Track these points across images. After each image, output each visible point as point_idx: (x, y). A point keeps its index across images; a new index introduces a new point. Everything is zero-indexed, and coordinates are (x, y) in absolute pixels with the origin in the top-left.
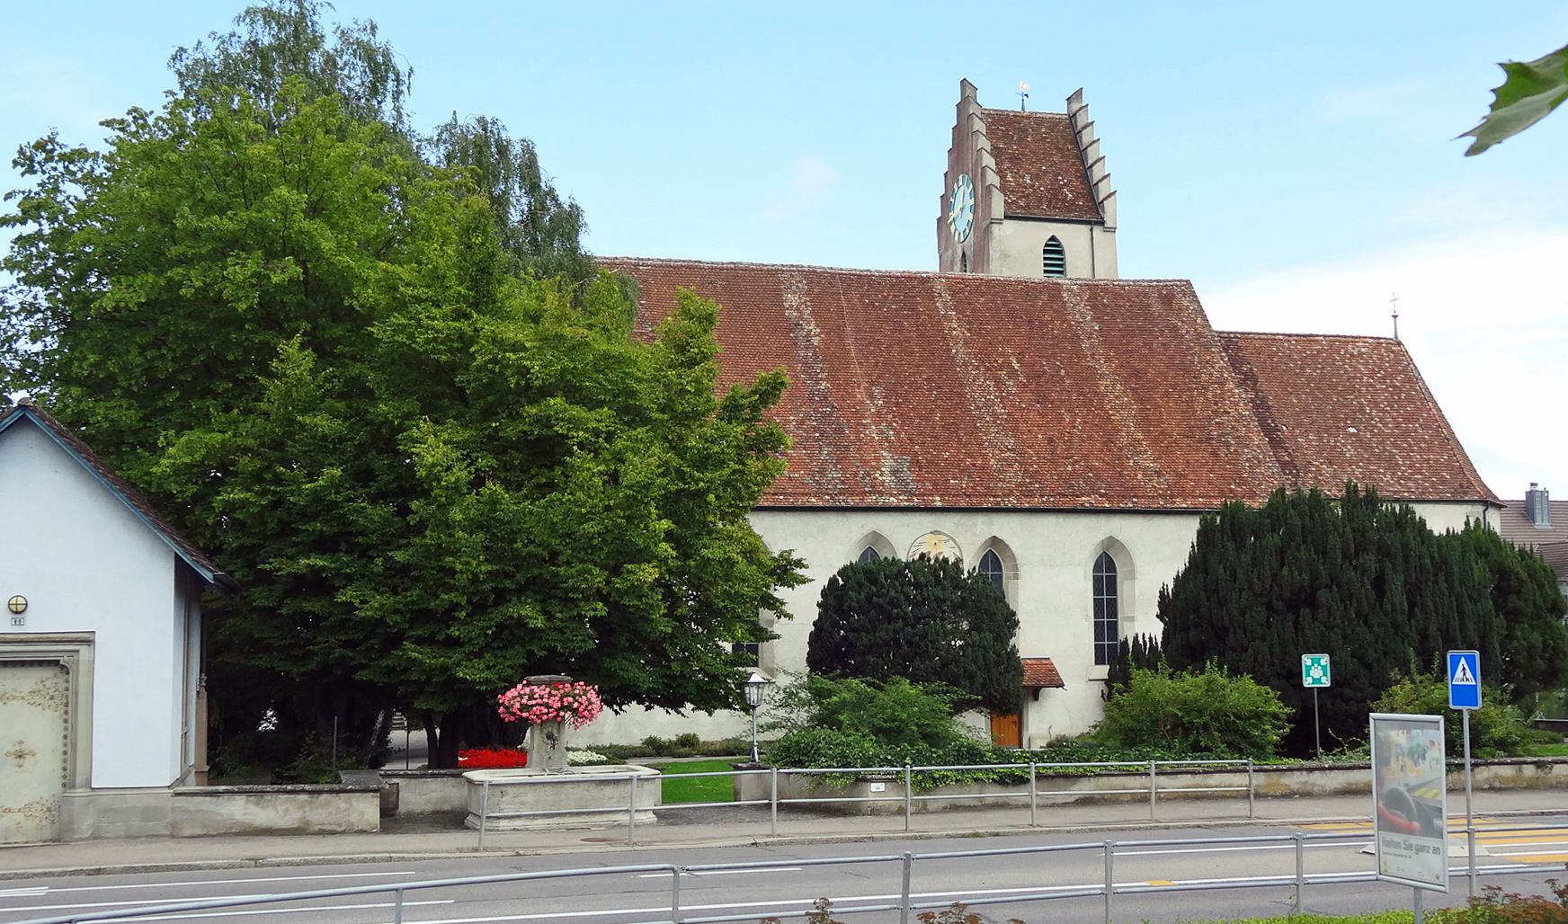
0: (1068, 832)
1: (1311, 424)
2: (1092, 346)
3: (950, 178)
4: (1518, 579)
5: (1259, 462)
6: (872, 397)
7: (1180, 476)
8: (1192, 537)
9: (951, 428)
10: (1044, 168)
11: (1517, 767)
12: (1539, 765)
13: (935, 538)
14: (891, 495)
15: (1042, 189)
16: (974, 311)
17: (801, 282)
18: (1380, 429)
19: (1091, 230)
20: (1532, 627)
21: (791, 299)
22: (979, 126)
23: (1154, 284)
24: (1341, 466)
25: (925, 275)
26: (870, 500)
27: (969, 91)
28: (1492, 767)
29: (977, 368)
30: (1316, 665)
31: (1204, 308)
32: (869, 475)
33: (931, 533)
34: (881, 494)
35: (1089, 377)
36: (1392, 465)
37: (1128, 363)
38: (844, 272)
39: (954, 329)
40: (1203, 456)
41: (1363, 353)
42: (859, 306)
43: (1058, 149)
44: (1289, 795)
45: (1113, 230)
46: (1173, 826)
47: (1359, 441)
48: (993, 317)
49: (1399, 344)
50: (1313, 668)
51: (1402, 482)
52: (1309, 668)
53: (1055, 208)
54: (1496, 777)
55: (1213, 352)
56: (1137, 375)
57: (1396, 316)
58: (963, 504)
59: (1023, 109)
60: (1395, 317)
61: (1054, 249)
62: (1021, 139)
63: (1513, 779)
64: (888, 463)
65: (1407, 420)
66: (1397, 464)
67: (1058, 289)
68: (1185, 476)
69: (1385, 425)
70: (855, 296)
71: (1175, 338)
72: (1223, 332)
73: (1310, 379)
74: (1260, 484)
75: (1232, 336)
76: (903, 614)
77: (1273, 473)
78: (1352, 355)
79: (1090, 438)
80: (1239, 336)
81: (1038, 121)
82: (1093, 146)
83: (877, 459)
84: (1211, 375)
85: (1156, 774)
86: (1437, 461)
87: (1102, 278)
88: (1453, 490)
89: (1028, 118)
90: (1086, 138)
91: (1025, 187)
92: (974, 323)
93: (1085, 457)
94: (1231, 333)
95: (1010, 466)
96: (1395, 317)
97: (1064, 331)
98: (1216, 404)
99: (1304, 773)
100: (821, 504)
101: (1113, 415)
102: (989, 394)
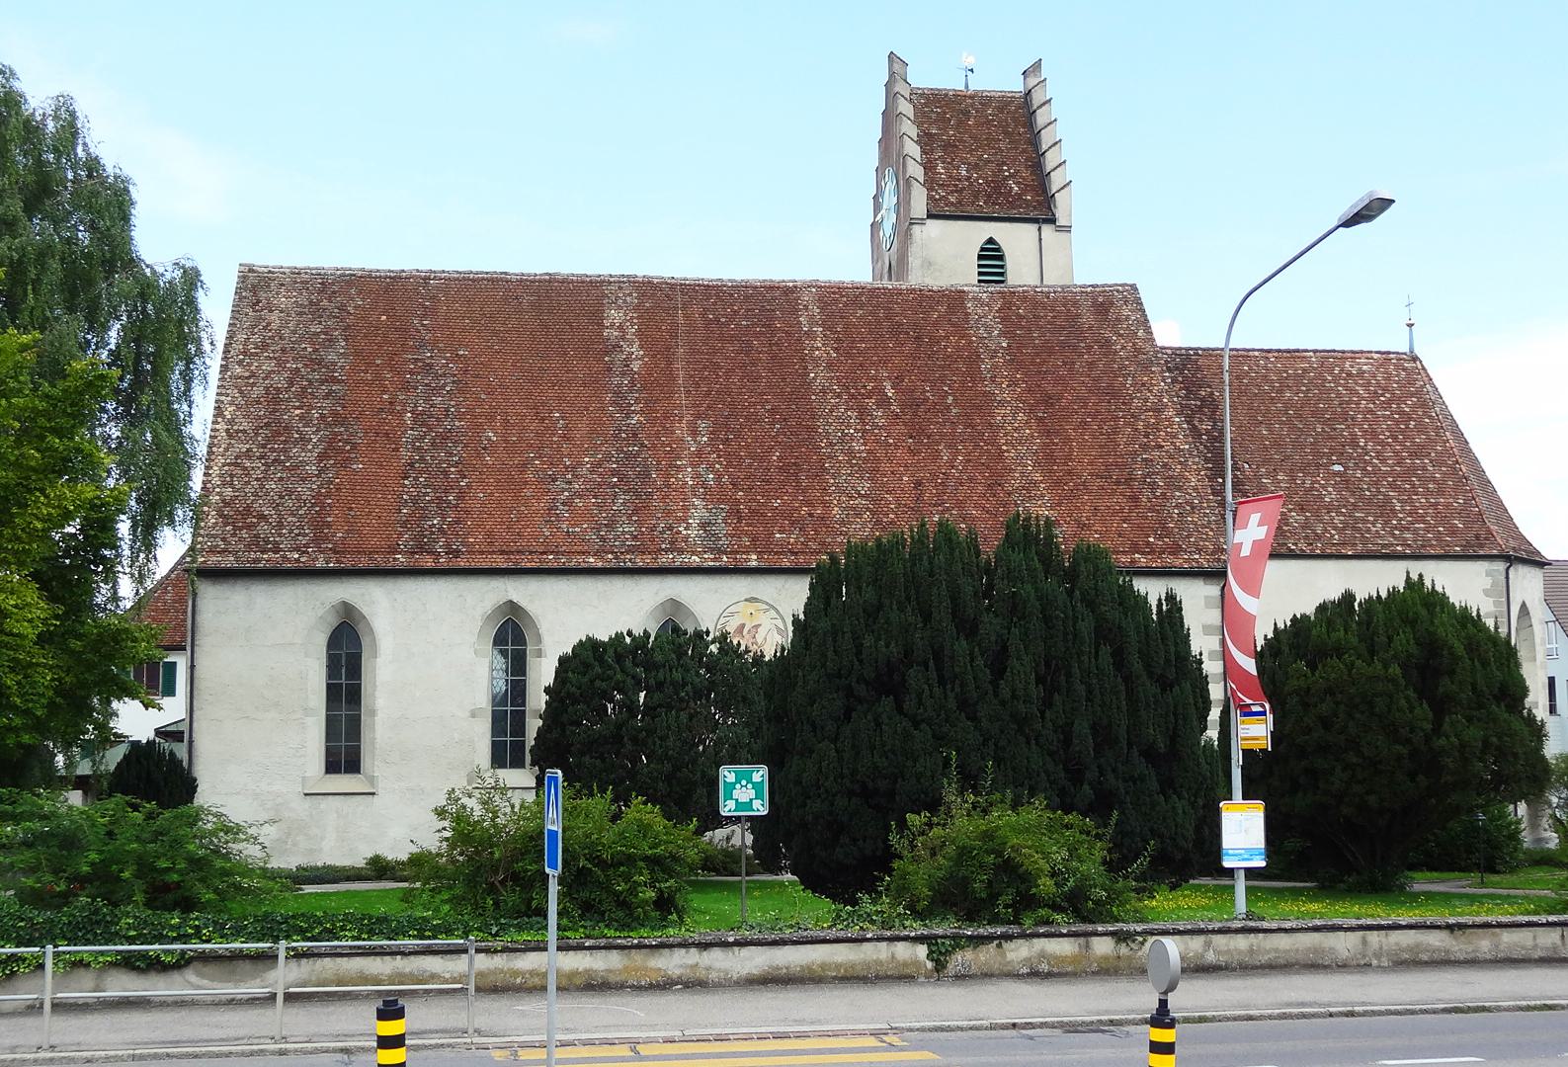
0: (89, 1061)
1: (1283, 460)
2: (995, 367)
3: (880, 172)
4: (1452, 654)
5: (1193, 508)
6: (694, 433)
7: (1082, 526)
8: (806, 593)
9: (790, 469)
10: (985, 156)
11: (1082, 940)
12: (1121, 937)
13: (751, 607)
14: (694, 553)
15: (981, 181)
16: (847, 326)
17: (630, 295)
18: (1374, 466)
19: (1040, 229)
20: (1469, 720)
21: (614, 315)
22: (905, 108)
23: (1089, 289)
24: (1316, 513)
25: (791, 284)
26: (665, 560)
27: (897, 67)
28: (1035, 940)
29: (839, 396)
30: (744, 782)
31: (1149, 317)
32: (670, 528)
33: (746, 600)
34: (681, 551)
35: (983, 405)
36: (1385, 511)
37: (1039, 386)
38: (687, 282)
39: (818, 349)
40: (1118, 501)
41: (1364, 372)
42: (700, 323)
43: (1006, 133)
44: (664, 985)
45: (1067, 229)
46: (296, 1051)
47: (1345, 481)
48: (870, 332)
49: (1415, 359)
50: (738, 786)
51: (1397, 532)
52: (731, 787)
53: (994, 204)
54: (1043, 955)
55: (1154, 372)
56: (1048, 401)
57: (1413, 325)
58: (786, 563)
59: (967, 86)
60: (1410, 326)
61: (991, 255)
62: (960, 123)
63: (1074, 960)
64: (699, 511)
65: (1413, 455)
66: (1393, 510)
67: (960, 297)
68: (1090, 527)
69: (1383, 461)
70: (696, 311)
71: (1105, 355)
72: (1180, 349)
73: (1288, 404)
74: (1189, 536)
75: (1192, 353)
76: (629, 702)
77: (1209, 522)
78: (1349, 375)
79: (971, 480)
80: (1200, 352)
81: (984, 100)
82: (1052, 126)
83: (685, 509)
84: (1146, 400)
85: (559, 949)
86: (1448, 506)
87: (1021, 284)
88: (1464, 543)
89: (972, 97)
90: (1041, 119)
91: (959, 180)
92: (844, 344)
93: (960, 505)
94: (1191, 349)
95: (859, 515)
96: (1410, 326)
97: (959, 349)
98: (1146, 436)
99: (693, 950)
100: (600, 565)
101: (1008, 451)
102: (849, 427)
